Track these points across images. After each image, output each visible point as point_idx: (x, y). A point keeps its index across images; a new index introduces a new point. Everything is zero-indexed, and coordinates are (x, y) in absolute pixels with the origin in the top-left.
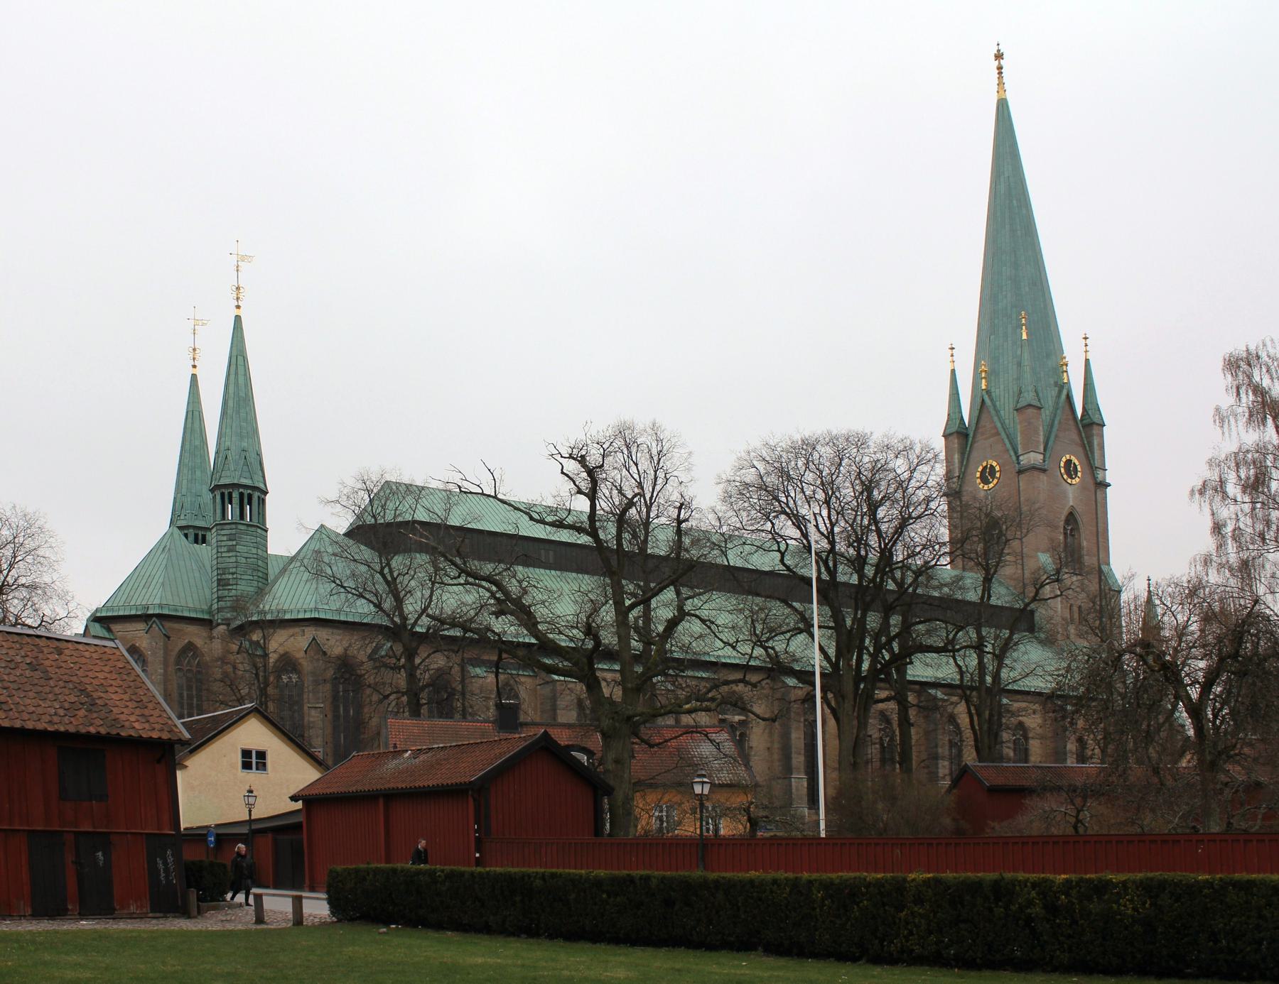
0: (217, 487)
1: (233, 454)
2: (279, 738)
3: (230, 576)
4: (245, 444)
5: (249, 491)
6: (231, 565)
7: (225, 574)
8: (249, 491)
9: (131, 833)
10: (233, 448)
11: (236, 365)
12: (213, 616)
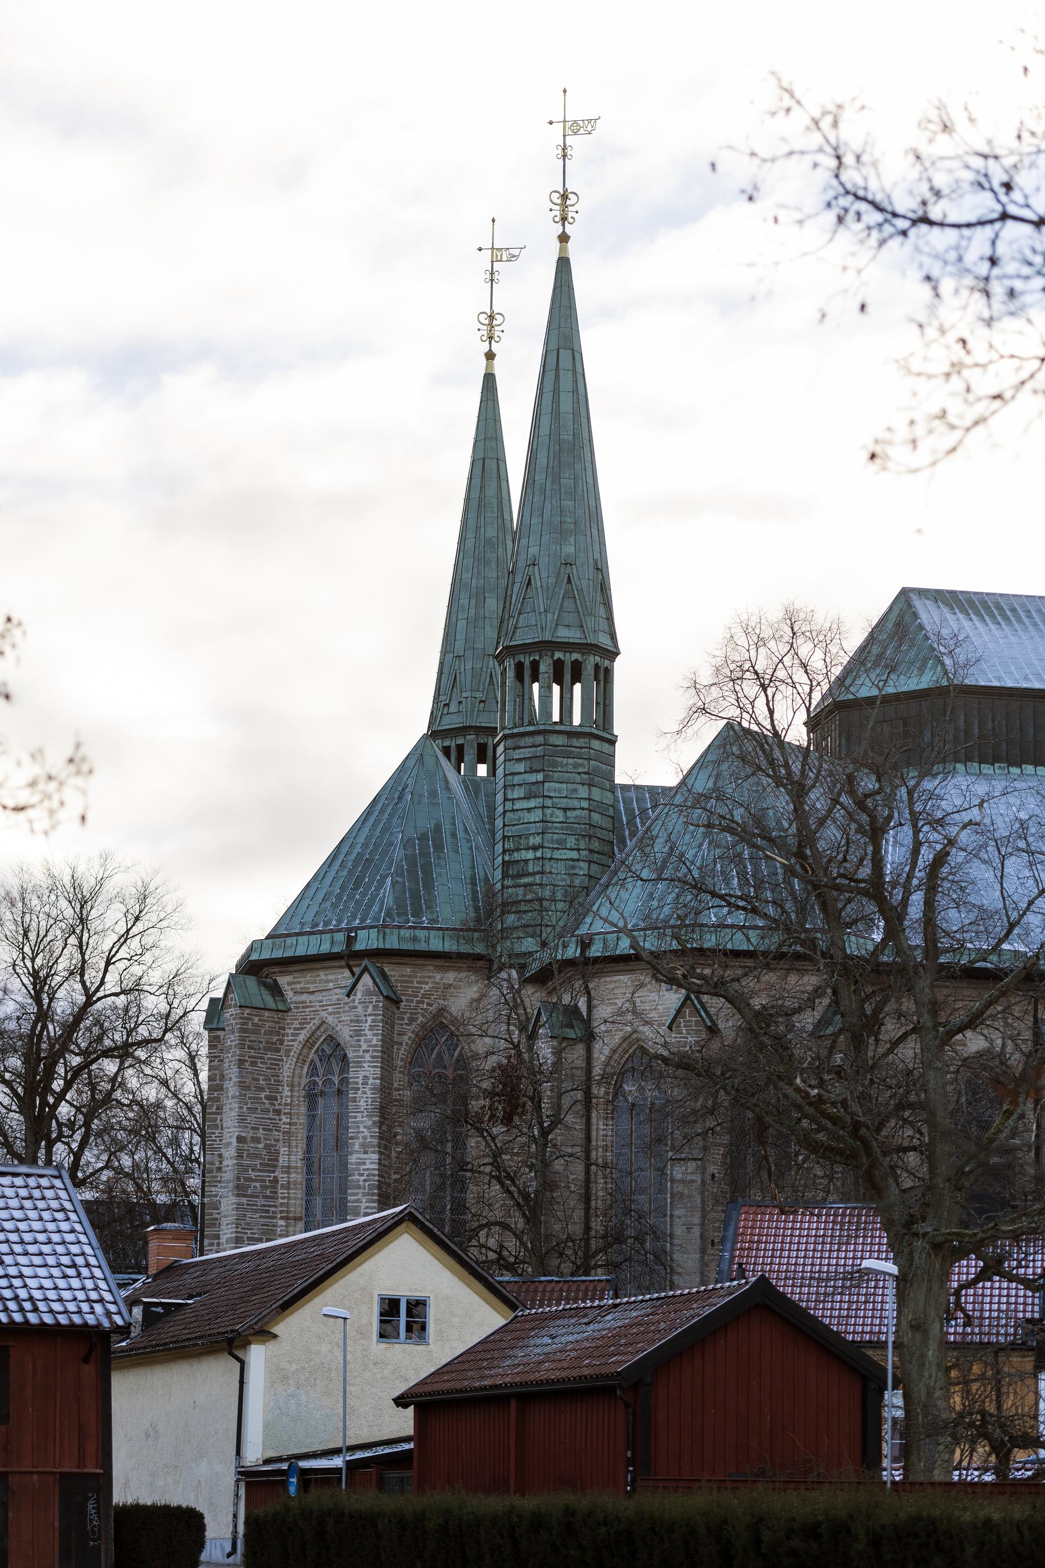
0: (510, 650)
1: (544, 575)
2: (453, 1272)
3: (530, 855)
4: (569, 549)
5: (576, 656)
6: (533, 829)
7: (518, 850)
8: (576, 656)
9: (38, 1473)
10: (544, 561)
11: (557, 369)
12: (494, 947)
